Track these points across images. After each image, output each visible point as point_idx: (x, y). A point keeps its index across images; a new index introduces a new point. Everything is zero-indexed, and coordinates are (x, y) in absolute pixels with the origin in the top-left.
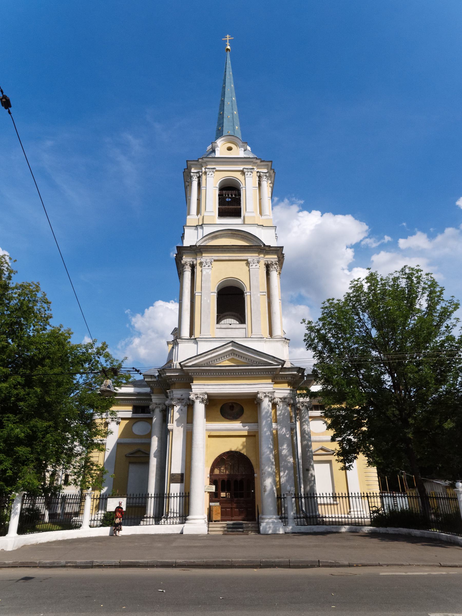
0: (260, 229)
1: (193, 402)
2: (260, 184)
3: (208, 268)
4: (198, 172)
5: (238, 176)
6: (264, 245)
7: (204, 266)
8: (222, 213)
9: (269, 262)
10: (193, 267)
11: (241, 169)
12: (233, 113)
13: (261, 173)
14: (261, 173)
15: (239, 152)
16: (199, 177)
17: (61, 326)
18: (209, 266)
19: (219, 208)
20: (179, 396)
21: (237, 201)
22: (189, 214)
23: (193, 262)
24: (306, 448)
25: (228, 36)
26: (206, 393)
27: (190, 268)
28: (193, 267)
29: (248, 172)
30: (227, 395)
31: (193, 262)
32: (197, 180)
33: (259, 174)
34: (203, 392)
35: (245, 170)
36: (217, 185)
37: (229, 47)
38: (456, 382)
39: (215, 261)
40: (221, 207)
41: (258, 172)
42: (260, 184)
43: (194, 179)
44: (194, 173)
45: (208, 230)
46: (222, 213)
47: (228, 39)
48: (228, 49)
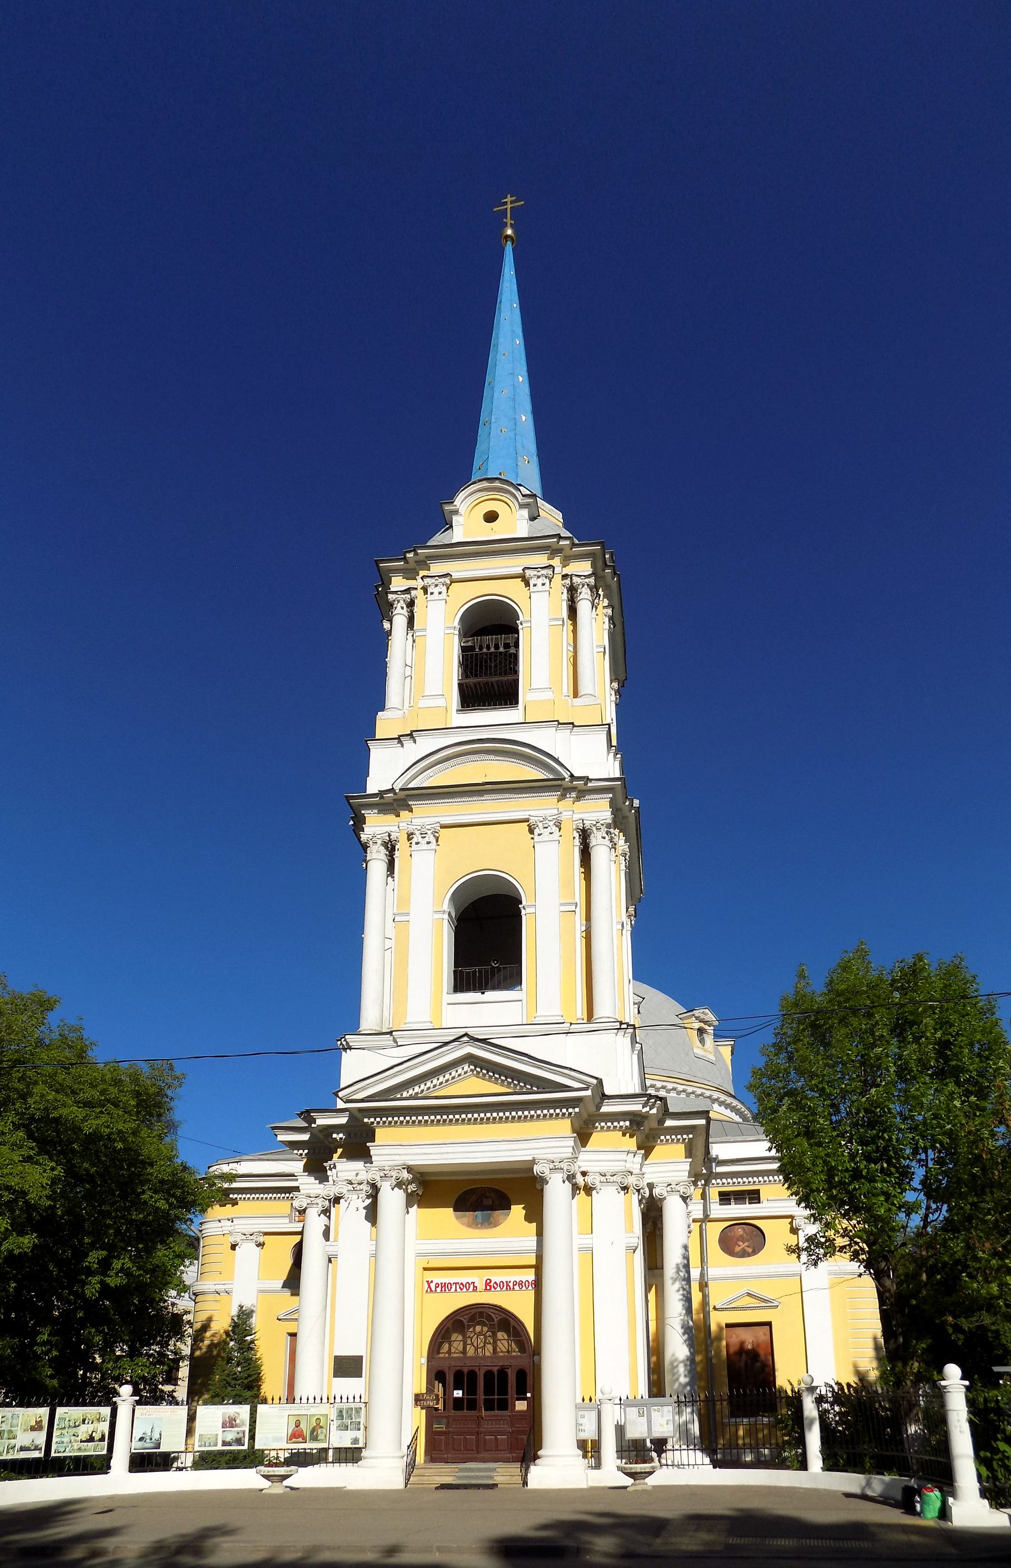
0: (564, 733)
1: (543, 1181)
2: (573, 612)
3: (426, 847)
4: (408, 591)
5: (512, 592)
6: (572, 776)
7: (417, 843)
8: (473, 697)
9: (587, 824)
10: (390, 847)
11: (519, 570)
12: (516, 421)
13: (575, 579)
14: (575, 579)
15: (514, 523)
16: (411, 604)
17: (46, 1005)
18: (428, 843)
19: (460, 685)
20: (351, 1176)
21: (508, 663)
22: (383, 709)
23: (389, 835)
24: (705, 1302)
25: (509, 199)
26: (409, 1169)
27: (383, 851)
28: (390, 847)
29: (539, 577)
30: (482, 1168)
31: (389, 835)
32: (405, 612)
33: (568, 581)
34: (398, 1163)
35: (528, 572)
36: (456, 623)
37: (509, 232)
38: (338, 1136)
39: (443, 827)
40: (472, 680)
41: (565, 577)
42: (573, 612)
43: (398, 610)
44: (396, 592)
45: (426, 745)
46: (473, 697)
47: (509, 206)
48: (507, 236)
